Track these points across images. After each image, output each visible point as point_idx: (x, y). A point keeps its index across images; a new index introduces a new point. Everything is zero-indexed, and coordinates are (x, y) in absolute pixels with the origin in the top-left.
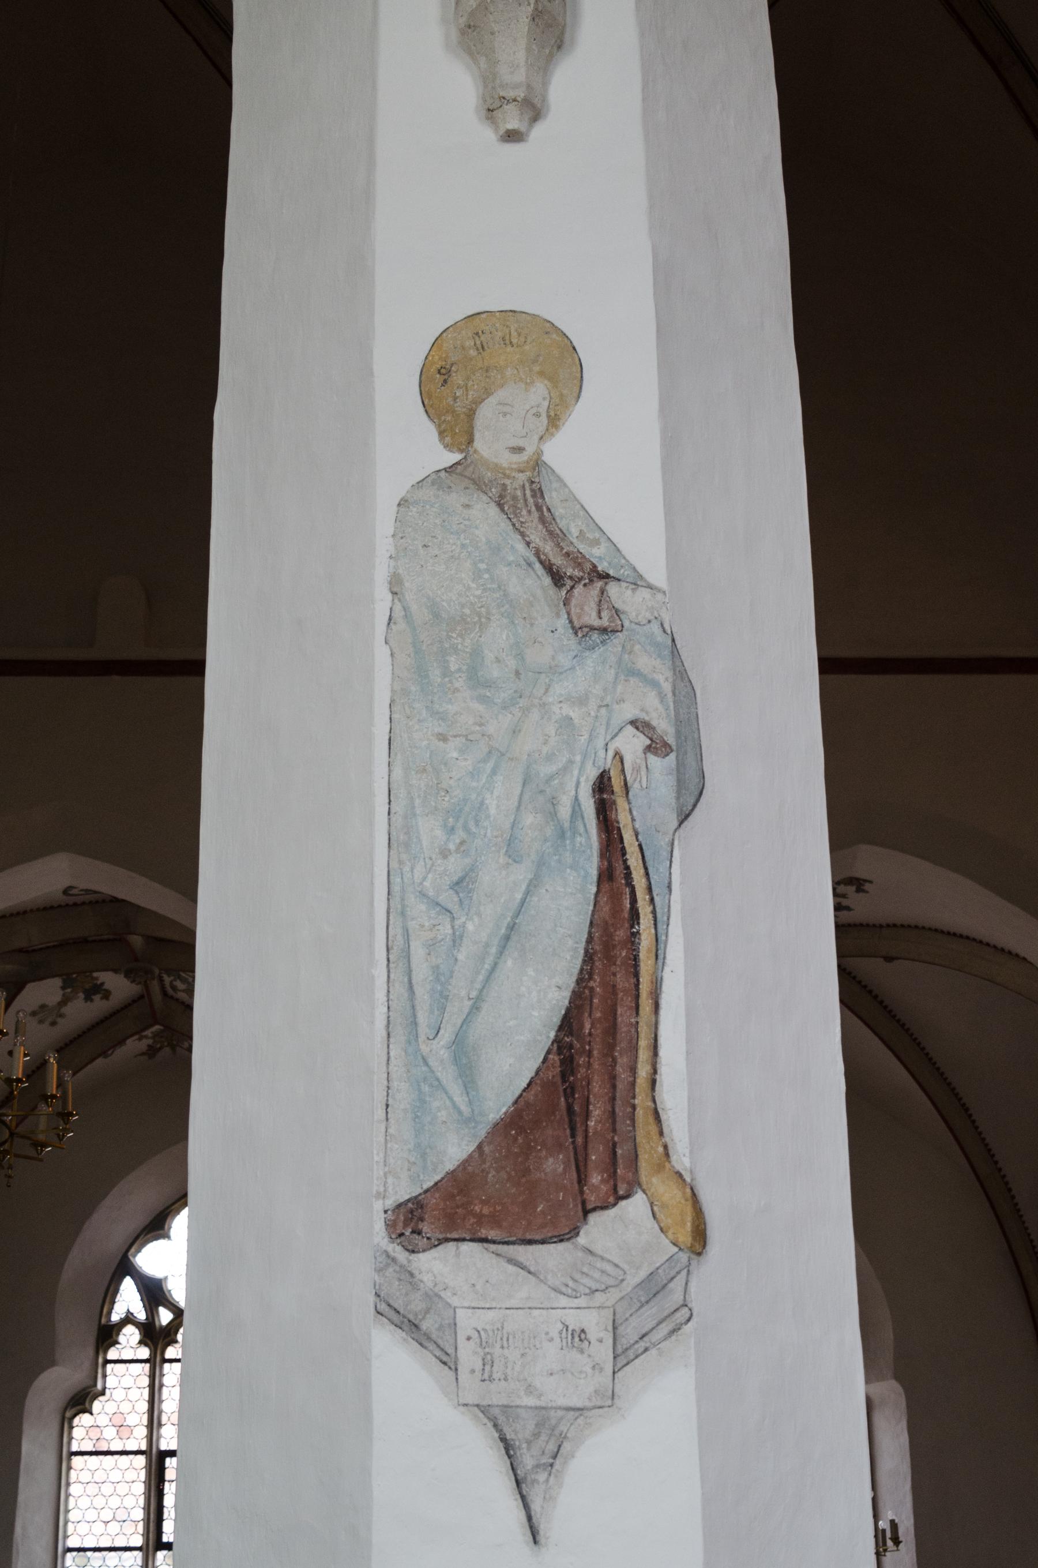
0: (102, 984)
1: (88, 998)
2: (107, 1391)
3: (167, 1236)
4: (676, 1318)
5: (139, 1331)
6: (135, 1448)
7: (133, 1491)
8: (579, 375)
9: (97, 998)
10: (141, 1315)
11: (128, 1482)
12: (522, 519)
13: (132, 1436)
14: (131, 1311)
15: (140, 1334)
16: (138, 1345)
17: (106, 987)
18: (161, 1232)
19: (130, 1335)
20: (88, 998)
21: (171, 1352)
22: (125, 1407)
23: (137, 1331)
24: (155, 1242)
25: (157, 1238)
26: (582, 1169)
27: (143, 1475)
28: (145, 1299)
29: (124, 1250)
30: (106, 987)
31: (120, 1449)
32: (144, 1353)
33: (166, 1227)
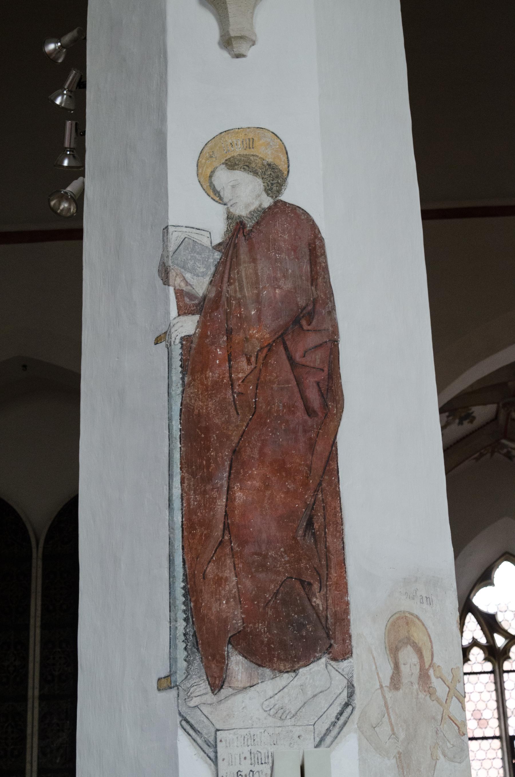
0: (472, 413)
1: (461, 423)
2: (467, 695)
3: (492, 584)
4: (172, 537)
5: (483, 651)
6: (492, 735)
7: (494, 765)
8: (213, 140)
9: (465, 423)
10: (483, 640)
11: (490, 759)
12: (275, 185)
13: (488, 727)
14: (476, 637)
15: (484, 653)
16: (484, 661)
17: (474, 415)
18: (489, 581)
19: (477, 654)
20: (461, 423)
21: (507, 666)
22: (481, 706)
23: (481, 652)
24: (485, 588)
25: (486, 586)
26: (171, 483)
27: (500, 754)
28: (486, 629)
29: (466, 596)
30: (474, 415)
31: (481, 735)
32: (488, 666)
33: (492, 578)
